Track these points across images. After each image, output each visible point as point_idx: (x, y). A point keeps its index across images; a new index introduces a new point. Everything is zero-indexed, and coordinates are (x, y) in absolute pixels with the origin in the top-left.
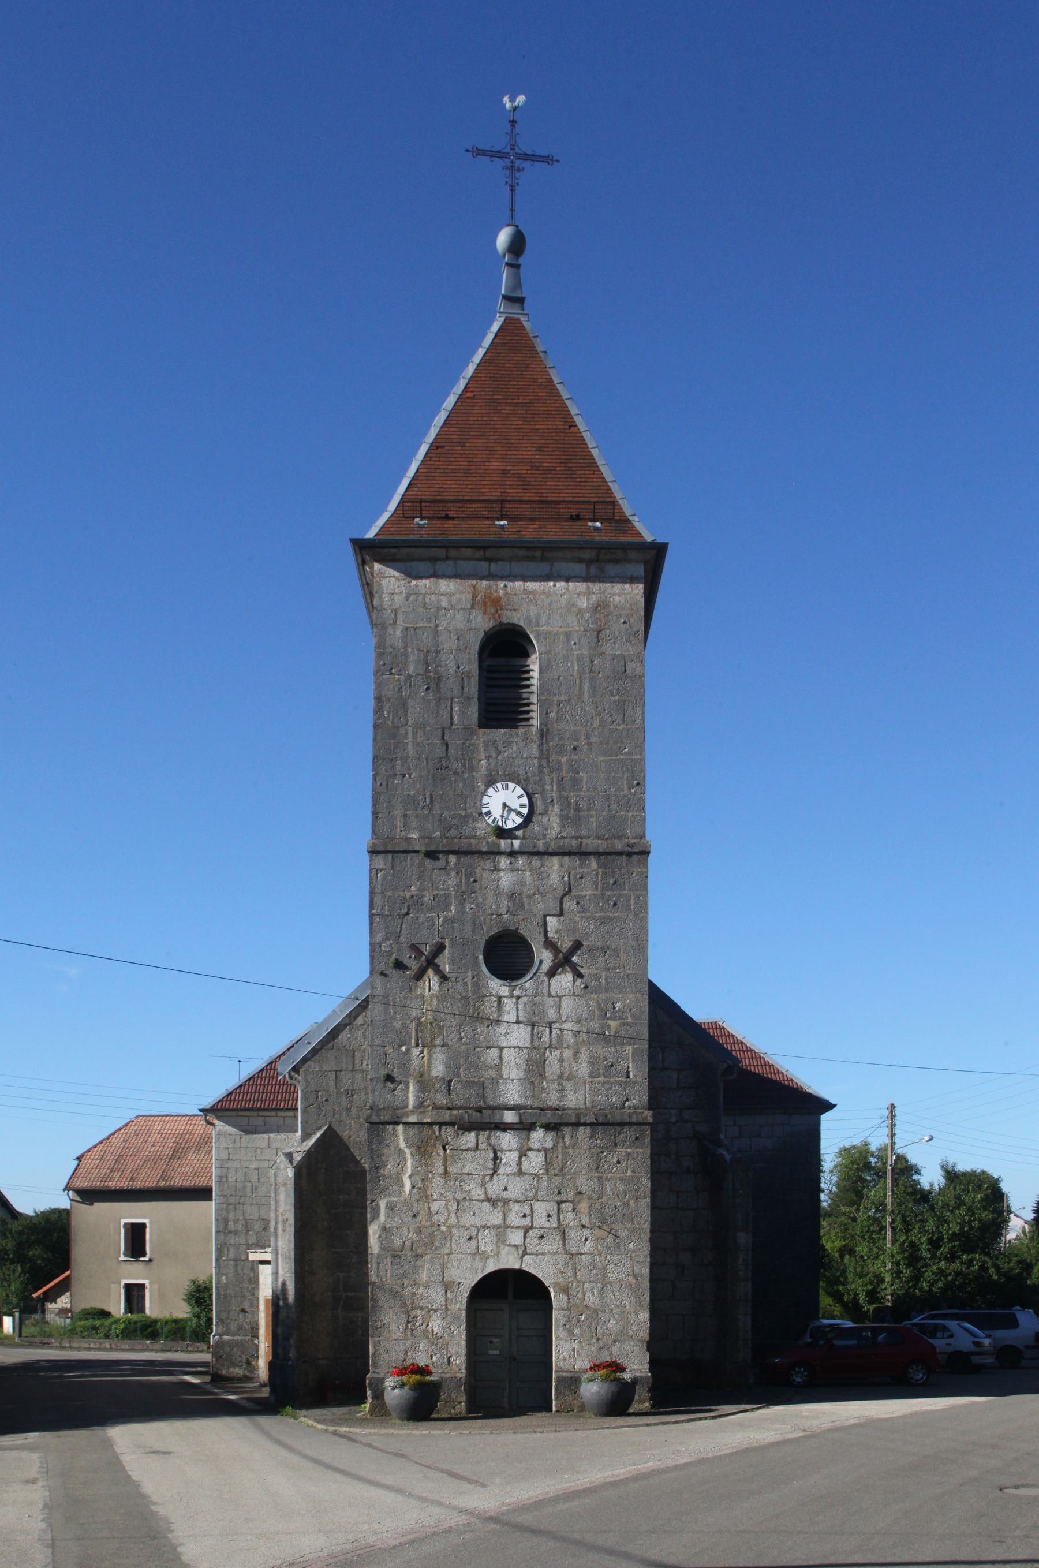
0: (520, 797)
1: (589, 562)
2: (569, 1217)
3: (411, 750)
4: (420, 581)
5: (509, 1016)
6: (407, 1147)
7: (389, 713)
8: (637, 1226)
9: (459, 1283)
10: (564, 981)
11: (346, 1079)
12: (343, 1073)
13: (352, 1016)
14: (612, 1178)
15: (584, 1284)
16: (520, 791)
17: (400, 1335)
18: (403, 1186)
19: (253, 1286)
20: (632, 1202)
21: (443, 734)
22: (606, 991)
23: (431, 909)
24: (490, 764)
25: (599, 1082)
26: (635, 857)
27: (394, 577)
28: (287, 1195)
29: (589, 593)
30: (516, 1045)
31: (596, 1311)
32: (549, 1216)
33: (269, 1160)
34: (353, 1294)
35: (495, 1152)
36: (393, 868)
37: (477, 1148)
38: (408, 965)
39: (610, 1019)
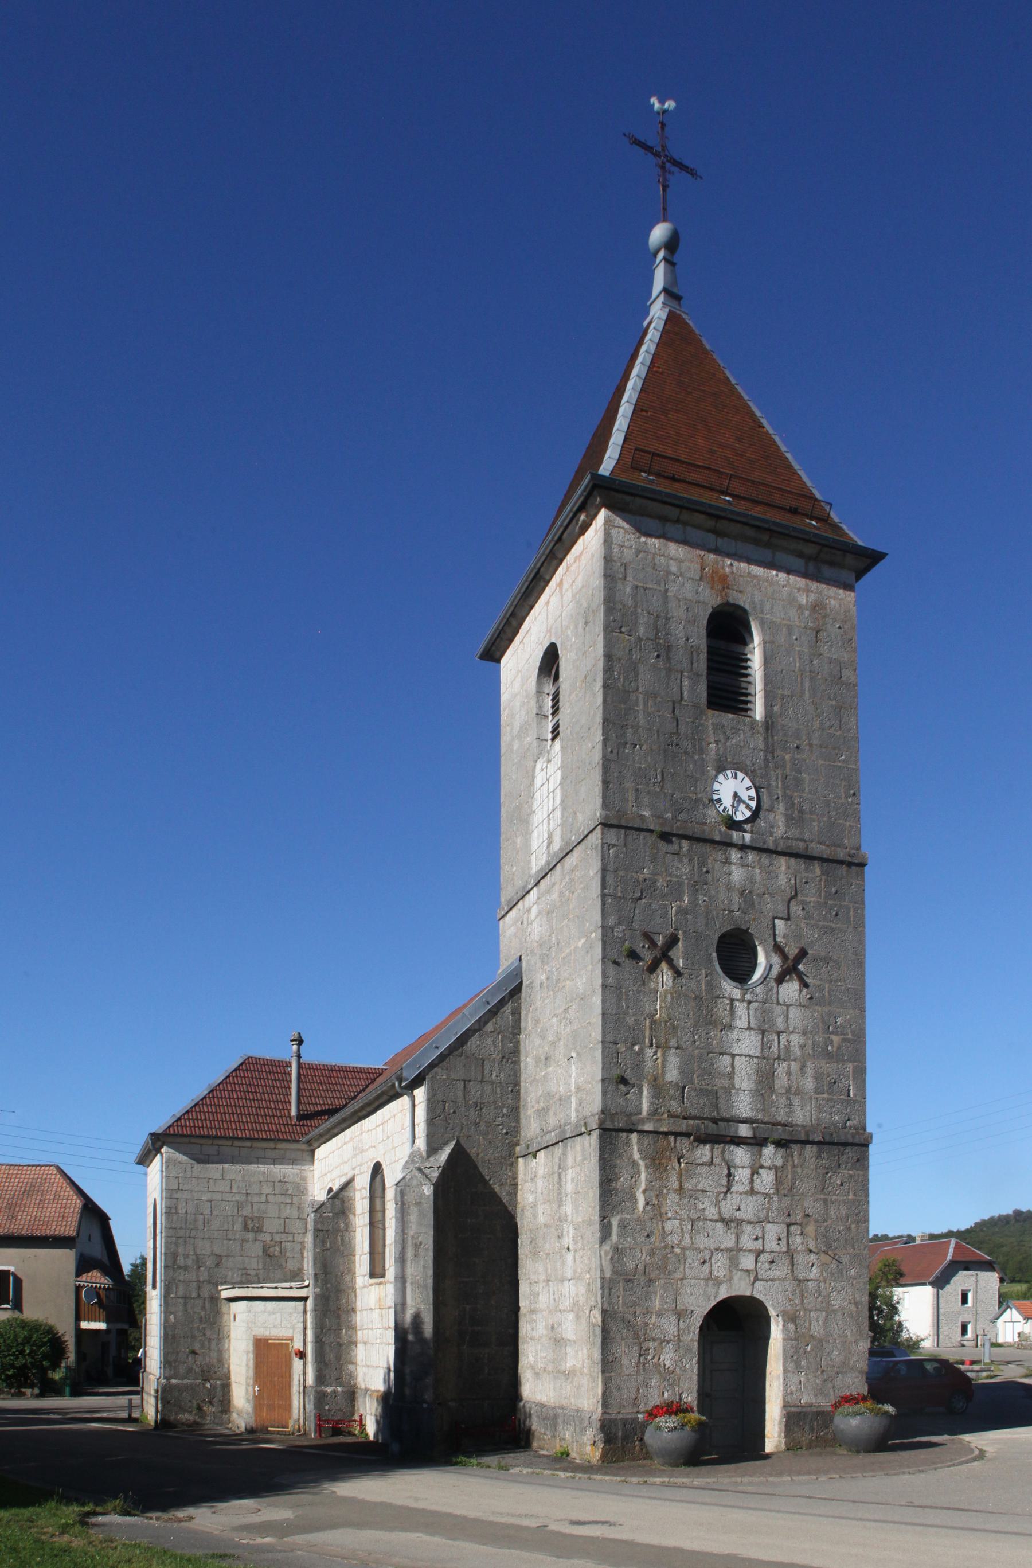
0: (748, 789)
1: (809, 558)
2: (797, 1241)
3: (642, 720)
4: (649, 539)
5: (741, 1022)
6: (641, 1158)
7: (619, 674)
8: (858, 1252)
9: (692, 1311)
10: (791, 989)
11: (474, 1090)
12: (472, 1083)
13: (482, 1022)
14: (836, 1200)
15: (810, 1312)
16: (748, 782)
17: (632, 1369)
18: (636, 1201)
19: (204, 1326)
20: (853, 1226)
21: (674, 708)
22: (830, 1004)
23: (664, 897)
24: (719, 749)
25: (824, 1099)
26: (853, 868)
27: (623, 528)
28: (422, 1215)
29: (808, 591)
30: (747, 1053)
31: (820, 1341)
32: (779, 1239)
33: (222, 1192)
34: (480, 1328)
35: (729, 1169)
36: (625, 845)
37: (711, 1163)
38: (642, 956)
39: (832, 1033)
